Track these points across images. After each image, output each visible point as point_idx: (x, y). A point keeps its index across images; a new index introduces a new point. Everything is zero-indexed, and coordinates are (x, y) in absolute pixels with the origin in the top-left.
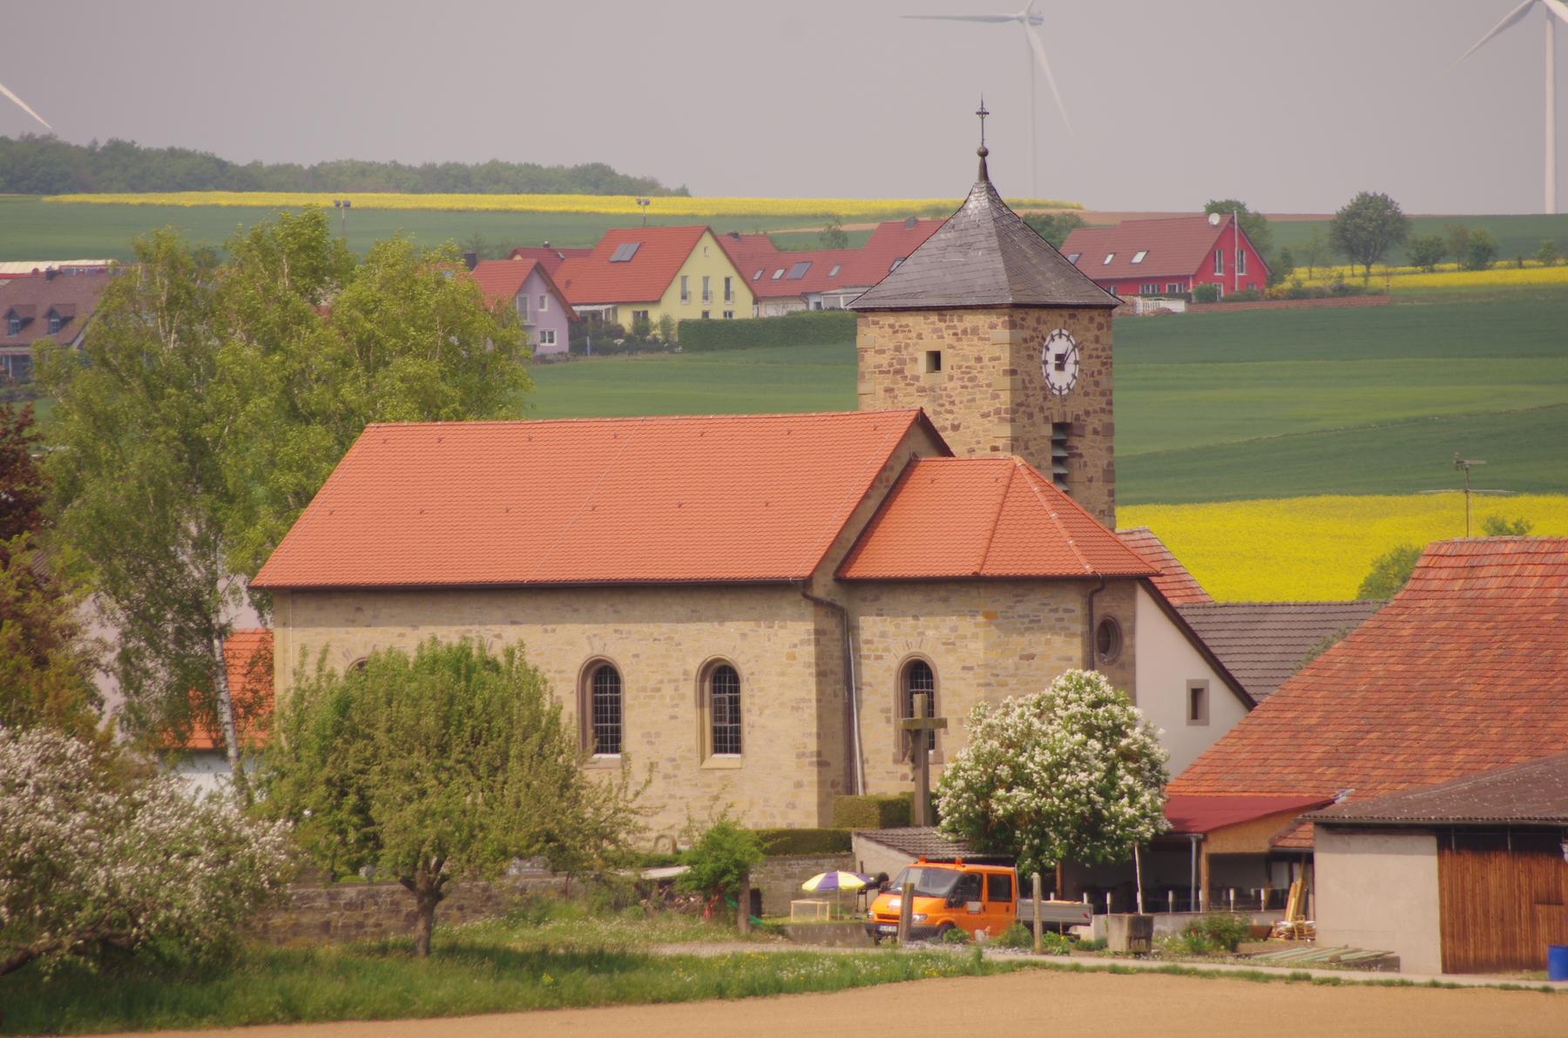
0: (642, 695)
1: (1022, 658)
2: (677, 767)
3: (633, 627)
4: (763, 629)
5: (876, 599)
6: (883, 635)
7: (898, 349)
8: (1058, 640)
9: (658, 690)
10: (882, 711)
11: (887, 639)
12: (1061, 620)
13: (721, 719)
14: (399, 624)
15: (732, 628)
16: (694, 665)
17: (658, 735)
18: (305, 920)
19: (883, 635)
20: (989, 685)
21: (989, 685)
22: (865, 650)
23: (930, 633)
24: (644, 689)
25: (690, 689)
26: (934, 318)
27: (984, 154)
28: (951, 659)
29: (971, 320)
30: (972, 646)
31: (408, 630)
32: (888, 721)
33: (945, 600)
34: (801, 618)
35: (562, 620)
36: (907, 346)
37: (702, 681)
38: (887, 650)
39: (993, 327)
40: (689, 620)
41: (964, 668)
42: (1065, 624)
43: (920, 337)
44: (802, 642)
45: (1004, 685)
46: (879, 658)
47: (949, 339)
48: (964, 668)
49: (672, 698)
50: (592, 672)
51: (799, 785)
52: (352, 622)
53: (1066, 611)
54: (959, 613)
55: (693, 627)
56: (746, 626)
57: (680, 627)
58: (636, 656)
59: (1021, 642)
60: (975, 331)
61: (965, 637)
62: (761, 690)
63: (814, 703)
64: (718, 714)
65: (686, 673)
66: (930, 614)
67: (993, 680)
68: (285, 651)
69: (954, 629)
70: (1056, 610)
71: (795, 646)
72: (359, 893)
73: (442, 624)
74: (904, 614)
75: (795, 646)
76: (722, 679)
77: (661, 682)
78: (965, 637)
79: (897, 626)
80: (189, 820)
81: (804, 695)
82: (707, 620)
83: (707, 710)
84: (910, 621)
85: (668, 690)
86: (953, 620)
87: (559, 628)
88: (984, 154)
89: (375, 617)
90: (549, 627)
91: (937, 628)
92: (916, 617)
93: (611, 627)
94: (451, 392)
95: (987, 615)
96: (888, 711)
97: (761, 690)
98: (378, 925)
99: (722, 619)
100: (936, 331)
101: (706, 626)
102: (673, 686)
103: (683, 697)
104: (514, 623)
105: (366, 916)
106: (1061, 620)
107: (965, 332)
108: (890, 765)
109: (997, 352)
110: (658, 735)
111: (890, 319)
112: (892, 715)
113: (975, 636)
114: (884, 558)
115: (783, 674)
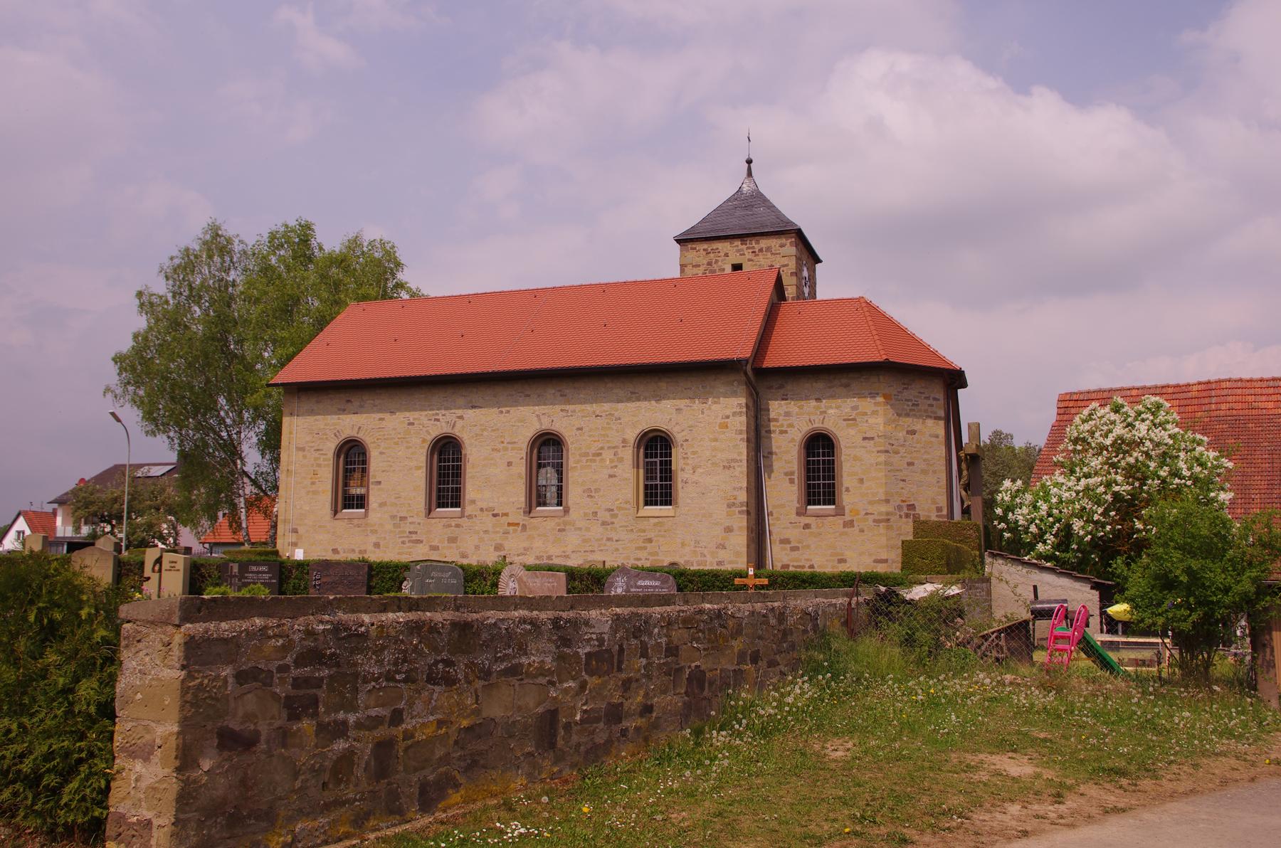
0: (584, 459)
1: (908, 432)
2: (615, 516)
3: (578, 407)
4: (697, 404)
5: (781, 387)
6: (787, 414)
7: (709, 264)
8: (930, 422)
9: (600, 454)
10: (786, 474)
11: (793, 418)
12: (931, 405)
13: (652, 478)
14: (380, 411)
15: (667, 405)
16: (632, 435)
17: (597, 490)
18: (496, 709)
19: (787, 414)
20: (887, 452)
21: (887, 452)
22: (773, 426)
23: (831, 411)
24: (586, 454)
25: (628, 454)
26: (738, 242)
27: (749, 162)
28: (852, 432)
29: (764, 243)
30: (871, 421)
31: (387, 416)
32: (792, 481)
33: (847, 386)
34: (734, 394)
35: (516, 404)
36: (717, 262)
37: (638, 448)
38: (791, 425)
39: (782, 246)
40: (629, 400)
41: (865, 439)
42: (934, 409)
43: (727, 255)
44: (734, 414)
45: (897, 453)
46: (782, 432)
47: (748, 255)
48: (865, 439)
49: (611, 461)
50: (538, 444)
51: (729, 530)
52: (343, 411)
53: (935, 399)
54: (861, 396)
55: (631, 406)
56: (682, 403)
57: (620, 405)
58: (581, 429)
59: (907, 422)
60: (768, 249)
61: (865, 414)
62: (694, 453)
63: (745, 463)
64: (649, 474)
65: (624, 441)
66: (833, 397)
67: (889, 448)
68: (291, 433)
69: (854, 408)
70: (927, 398)
71: (728, 417)
72: (617, 619)
73: (415, 410)
74: (807, 398)
75: (728, 417)
76: (656, 446)
77: (602, 448)
78: (865, 414)
79: (801, 407)
80: (262, 306)
81: (735, 456)
82: (645, 399)
83: (641, 471)
84: (813, 403)
85: (608, 455)
86: (854, 401)
87: (512, 410)
88: (749, 162)
89: (361, 406)
90: (504, 410)
91: (838, 407)
92: (818, 400)
93: (558, 408)
94: (26, 824)
95: (885, 396)
96: (792, 473)
97: (694, 453)
98: (647, 709)
99: (659, 398)
100: (738, 251)
101: (644, 404)
102: (612, 451)
103: (621, 460)
104: (473, 407)
105: (627, 685)
106: (931, 405)
107: (761, 250)
108: (793, 517)
109: (785, 261)
110: (597, 490)
111: (703, 246)
112: (795, 477)
113: (874, 413)
114: (770, 362)
115: (716, 440)
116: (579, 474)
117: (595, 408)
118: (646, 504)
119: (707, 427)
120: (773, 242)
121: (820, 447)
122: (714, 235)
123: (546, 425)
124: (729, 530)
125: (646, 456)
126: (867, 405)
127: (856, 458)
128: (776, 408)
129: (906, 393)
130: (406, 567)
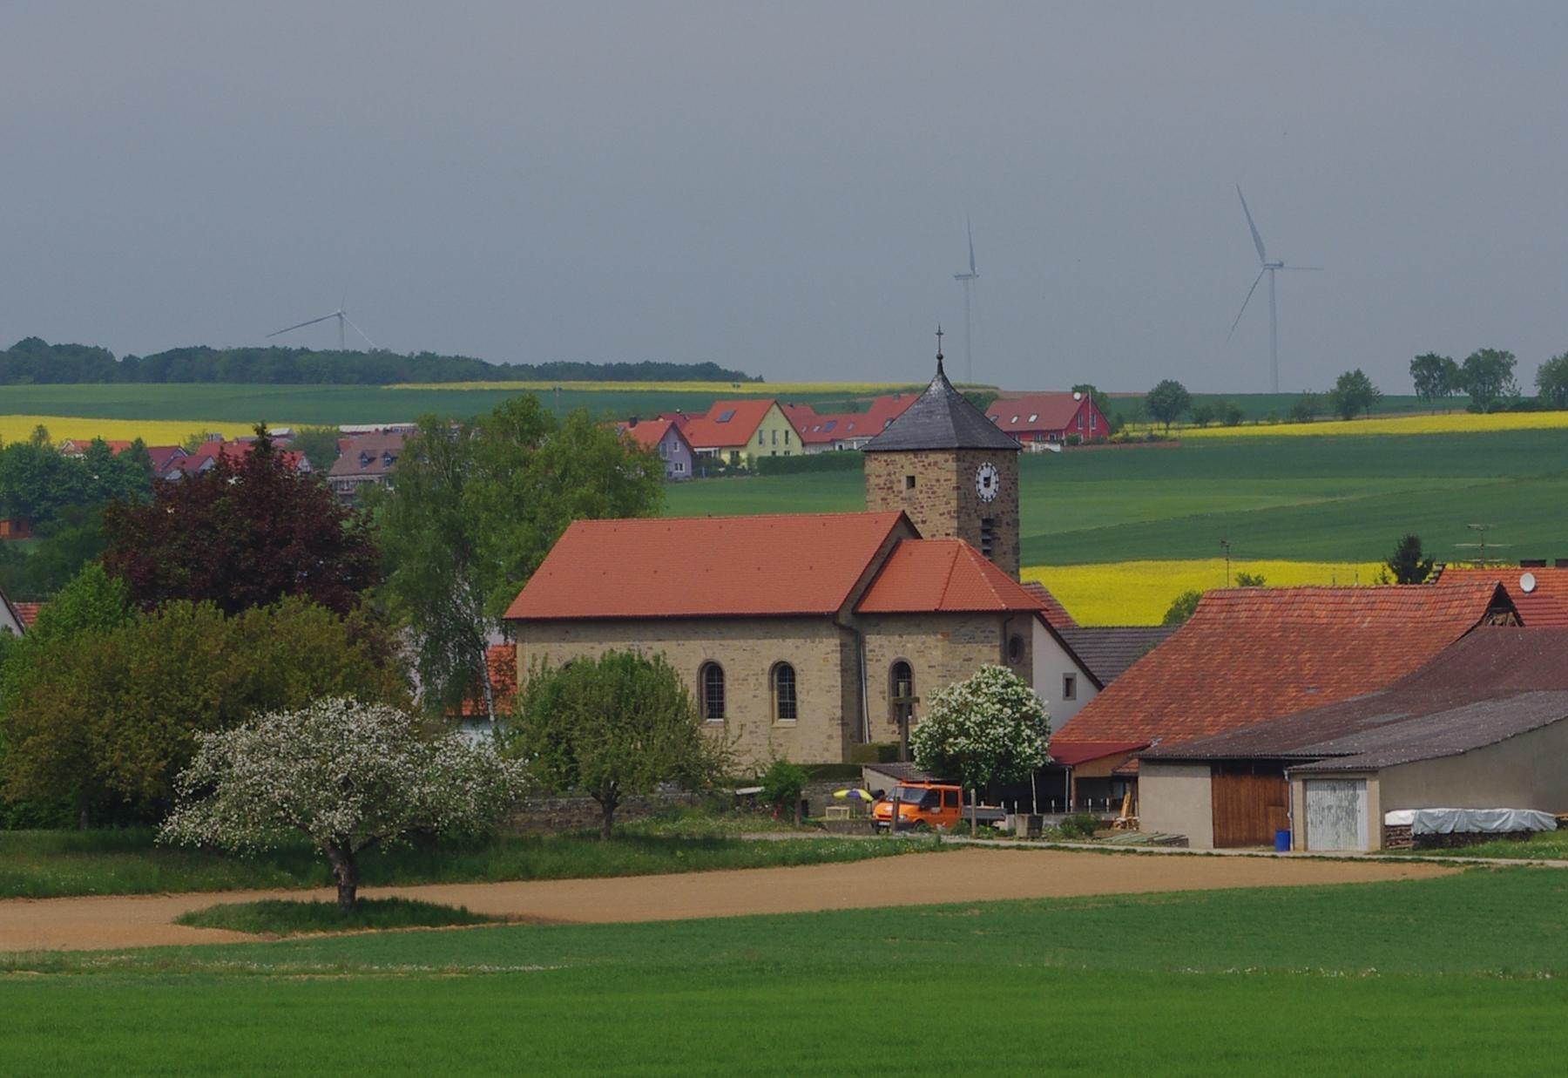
6: (881, 646)
11: (883, 649)
15: (790, 642)
16: (767, 665)
19: (881, 646)
25: (765, 680)
27: (940, 358)
29: (933, 457)
35: (688, 638)
47: (920, 469)
51: (830, 737)
56: (799, 642)
60: (936, 463)
64: (782, 695)
76: (784, 674)
84: (897, 638)
85: (752, 680)
88: (940, 358)
99: (784, 638)
116: (733, 696)
117: (737, 643)
118: (781, 717)
119: (817, 659)
120: (939, 457)
121: (902, 671)
122: (891, 447)
123: (709, 656)
124: (830, 737)
125: (780, 680)
126: (931, 640)
127: (925, 682)
128: (873, 641)
129: (963, 630)
130: (273, 382)
